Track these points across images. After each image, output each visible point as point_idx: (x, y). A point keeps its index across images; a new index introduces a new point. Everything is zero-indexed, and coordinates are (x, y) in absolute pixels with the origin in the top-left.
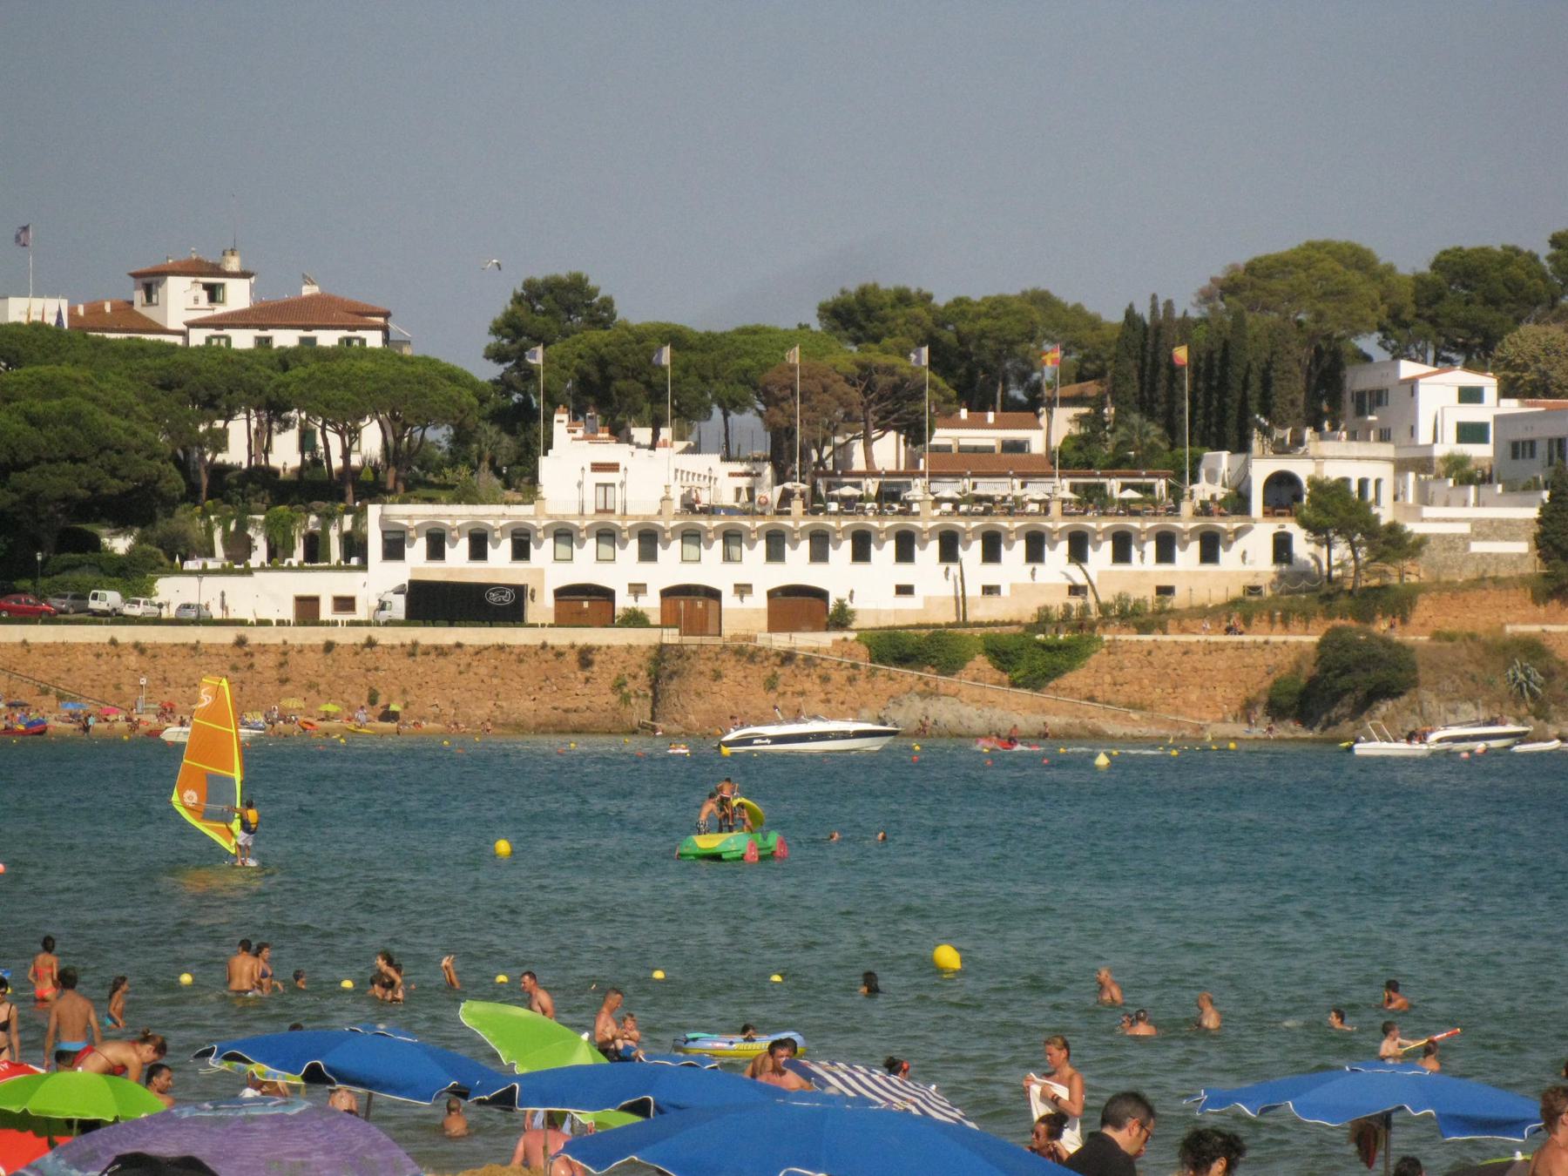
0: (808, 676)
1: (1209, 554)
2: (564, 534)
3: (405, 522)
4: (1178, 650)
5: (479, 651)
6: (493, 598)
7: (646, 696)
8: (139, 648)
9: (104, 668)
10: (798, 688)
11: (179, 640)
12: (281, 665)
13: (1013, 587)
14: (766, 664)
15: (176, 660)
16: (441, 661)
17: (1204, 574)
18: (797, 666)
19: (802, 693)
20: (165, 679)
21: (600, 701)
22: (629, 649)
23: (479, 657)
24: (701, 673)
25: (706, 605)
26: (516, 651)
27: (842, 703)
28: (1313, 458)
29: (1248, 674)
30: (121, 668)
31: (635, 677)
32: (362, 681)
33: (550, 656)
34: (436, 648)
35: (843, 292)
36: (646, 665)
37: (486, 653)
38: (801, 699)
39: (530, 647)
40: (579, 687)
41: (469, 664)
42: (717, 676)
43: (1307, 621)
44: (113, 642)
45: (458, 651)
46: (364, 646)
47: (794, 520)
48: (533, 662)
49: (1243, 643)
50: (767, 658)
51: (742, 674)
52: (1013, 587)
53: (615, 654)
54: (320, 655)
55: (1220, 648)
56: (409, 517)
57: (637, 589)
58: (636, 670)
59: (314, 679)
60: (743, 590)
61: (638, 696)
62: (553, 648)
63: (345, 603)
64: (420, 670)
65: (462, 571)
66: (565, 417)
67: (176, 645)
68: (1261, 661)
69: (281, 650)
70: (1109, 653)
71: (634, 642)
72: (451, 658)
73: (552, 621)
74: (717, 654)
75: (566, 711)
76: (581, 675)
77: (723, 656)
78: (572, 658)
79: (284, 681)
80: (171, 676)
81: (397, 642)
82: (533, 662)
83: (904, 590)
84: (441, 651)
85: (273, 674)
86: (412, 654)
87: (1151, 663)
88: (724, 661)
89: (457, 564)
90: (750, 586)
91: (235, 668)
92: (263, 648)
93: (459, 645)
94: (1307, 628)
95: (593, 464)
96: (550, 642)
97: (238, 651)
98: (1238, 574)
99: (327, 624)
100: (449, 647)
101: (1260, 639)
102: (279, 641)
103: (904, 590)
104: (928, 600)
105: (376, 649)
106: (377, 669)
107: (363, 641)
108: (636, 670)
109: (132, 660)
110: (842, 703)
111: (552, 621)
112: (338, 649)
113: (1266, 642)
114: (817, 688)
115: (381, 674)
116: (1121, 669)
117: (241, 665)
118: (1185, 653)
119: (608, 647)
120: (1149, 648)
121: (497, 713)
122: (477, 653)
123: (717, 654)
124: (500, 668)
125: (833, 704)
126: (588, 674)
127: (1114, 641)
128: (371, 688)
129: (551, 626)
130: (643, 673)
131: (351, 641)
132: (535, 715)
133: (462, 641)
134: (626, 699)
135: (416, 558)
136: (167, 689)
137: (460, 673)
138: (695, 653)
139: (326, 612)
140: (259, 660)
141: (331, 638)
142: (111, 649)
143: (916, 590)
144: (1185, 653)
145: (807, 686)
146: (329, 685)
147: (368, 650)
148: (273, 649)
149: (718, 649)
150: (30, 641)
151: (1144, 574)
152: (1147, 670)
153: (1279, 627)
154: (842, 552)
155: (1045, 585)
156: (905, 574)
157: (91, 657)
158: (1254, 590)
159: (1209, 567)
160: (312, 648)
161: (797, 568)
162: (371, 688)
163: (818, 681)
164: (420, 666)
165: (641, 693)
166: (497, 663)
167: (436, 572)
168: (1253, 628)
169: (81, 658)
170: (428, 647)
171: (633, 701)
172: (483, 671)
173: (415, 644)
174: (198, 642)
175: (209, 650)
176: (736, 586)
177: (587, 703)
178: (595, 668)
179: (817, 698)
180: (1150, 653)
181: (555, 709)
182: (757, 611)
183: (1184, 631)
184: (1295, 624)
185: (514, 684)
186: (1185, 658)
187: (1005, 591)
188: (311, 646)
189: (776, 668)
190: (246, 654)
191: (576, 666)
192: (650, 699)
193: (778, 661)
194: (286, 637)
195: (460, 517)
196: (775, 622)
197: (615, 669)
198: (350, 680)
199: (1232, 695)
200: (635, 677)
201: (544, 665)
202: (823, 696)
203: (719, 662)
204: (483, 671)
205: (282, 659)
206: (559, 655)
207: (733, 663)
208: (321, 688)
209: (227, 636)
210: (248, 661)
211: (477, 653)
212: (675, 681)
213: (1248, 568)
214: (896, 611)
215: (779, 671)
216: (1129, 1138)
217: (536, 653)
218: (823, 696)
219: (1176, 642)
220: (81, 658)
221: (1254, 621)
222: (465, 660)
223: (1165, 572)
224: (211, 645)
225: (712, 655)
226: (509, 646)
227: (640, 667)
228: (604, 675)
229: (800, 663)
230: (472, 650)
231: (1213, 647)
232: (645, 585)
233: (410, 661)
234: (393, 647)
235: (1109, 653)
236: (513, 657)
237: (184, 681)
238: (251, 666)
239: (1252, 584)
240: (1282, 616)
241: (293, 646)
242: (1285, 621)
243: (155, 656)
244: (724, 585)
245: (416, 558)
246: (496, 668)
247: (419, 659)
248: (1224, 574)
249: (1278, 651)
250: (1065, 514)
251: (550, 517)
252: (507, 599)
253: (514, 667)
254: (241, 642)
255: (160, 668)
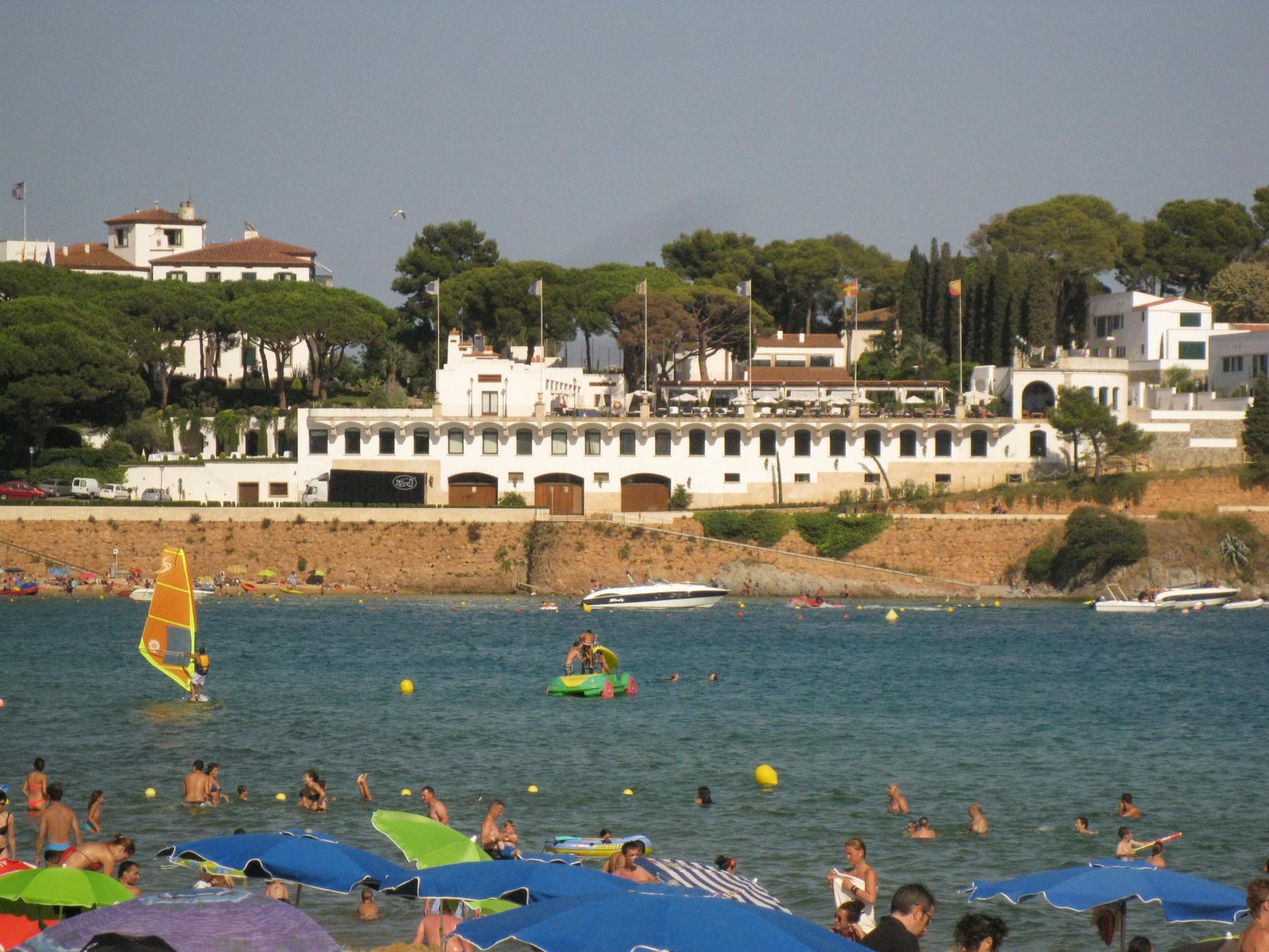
0: (654, 547)
1: (979, 448)
2: (457, 433)
3: (328, 423)
4: (954, 526)
5: (388, 527)
6: (399, 484)
7: (523, 563)
8: (113, 525)
9: (84, 540)
10: (646, 557)
11: (145, 518)
12: (228, 538)
13: (820, 475)
14: (620, 537)
15: (142, 534)
16: (357, 535)
17: (975, 465)
18: (645, 539)
19: (649, 561)
20: (133, 550)
21: (486, 568)
22: (509, 525)
23: (387, 532)
24: (568, 545)
25: (571, 490)
26: (418, 527)
27: (682, 569)
28: (1063, 371)
29: (1010, 545)
30: (98, 540)
31: (514, 548)
32: (293, 551)
33: (445, 531)
34: (353, 524)
35: (682, 237)
36: (523, 538)
37: (393, 529)
38: (648, 566)
39: (429, 524)
40: (469, 556)
41: (380, 538)
42: (581, 547)
43: (1058, 503)
44: (92, 520)
45: (371, 527)
46: (295, 523)
47: (643, 421)
48: (431, 536)
49: (1006, 520)
50: (621, 533)
51: (600, 545)
52: (820, 475)
53: (498, 529)
54: (259, 530)
55: (987, 524)
56: (331, 419)
57: (516, 477)
58: (515, 542)
59: (254, 550)
60: (601, 477)
61: (516, 564)
62: (447, 524)
63: (279, 489)
64: (340, 542)
65: (374, 462)
66: (457, 338)
67: (142, 522)
68: (1020, 535)
69: (227, 526)
70: (898, 529)
71: (513, 520)
72: (365, 532)
73: (447, 503)
74: (580, 529)
75: (458, 575)
76: (470, 547)
77: (585, 531)
78: (463, 532)
79: (229, 552)
80: (138, 547)
81: (321, 520)
82: (431, 536)
83: (732, 478)
84: (357, 527)
85: (221, 546)
86: (333, 530)
87: (931, 537)
88: (586, 535)
89: (370, 457)
90: (607, 474)
91: (190, 541)
92: (213, 525)
93: (371, 522)
94: (1058, 508)
95: (480, 376)
96: (445, 520)
97: (193, 527)
98: (1002, 465)
99: (265, 505)
100: (364, 524)
101: (1020, 517)
102: (226, 519)
103: (732, 478)
104: (751, 486)
105: (304, 525)
106: (305, 542)
107: (294, 519)
108: (515, 542)
109: (107, 534)
110: (682, 569)
111: (447, 503)
112: (273, 525)
113: (1025, 520)
114: (661, 557)
115: (309, 545)
116: (907, 542)
117: (195, 539)
118: (959, 529)
119: (492, 524)
120: (930, 524)
121: (402, 577)
122: (386, 529)
123: (580, 529)
124: (405, 541)
125: (675, 570)
126: (476, 546)
127: (902, 519)
128: (300, 557)
129: (446, 507)
130: (520, 545)
131: (284, 519)
132: (433, 579)
133: (374, 519)
134: (506, 566)
135: (337, 452)
136: (135, 558)
137: (373, 545)
138: (562, 528)
139: (264, 495)
140: (209, 534)
141: (268, 517)
142: (90, 525)
143: (741, 478)
144: (959, 529)
145: (654, 555)
146: (266, 554)
147: (297, 526)
148: (221, 525)
149: (581, 526)
150: (24, 519)
151: (926, 465)
152: (928, 543)
153: (1035, 507)
154: (682, 447)
155: (846, 474)
156: (732, 464)
157: (73, 532)
158: (1015, 478)
159: (978, 459)
160: (253, 524)
161: (645, 460)
162: (300, 557)
163: (662, 551)
164: (340, 539)
165: (519, 561)
166: (403, 537)
167: (353, 463)
168: (1014, 508)
169: (65, 533)
170: (346, 523)
171: (512, 567)
172: (391, 543)
173: (336, 522)
174: (160, 520)
175: (169, 526)
176: (596, 474)
177: (475, 569)
178: (482, 541)
179: (661, 565)
180: (930, 529)
181: (449, 574)
182: (612, 495)
183: (958, 511)
184: (1048, 505)
185: (416, 554)
186: (959, 533)
187: (813, 479)
188: (251, 523)
189: (628, 541)
190: (199, 530)
191: (466, 539)
192: (526, 566)
193: (630, 535)
194: (232, 516)
195: (372, 418)
196: (628, 504)
197: (498, 542)
198: (283, 550)
199: (997, 563)
200: (514, 548)
201: (440, 539)
202: (666, 563)
203: (582, 536)
204: (391, 543)
205: (228, 533)
206: (453, 530)
207: (593, 536)
208: (260, 557)
209: (184, 515)
210: (200, 535)
211: (386, 529)
212: (547, 551)
213: (1010, 460)
214: (725, 495)
215: (631, 543)
216: (913, 921)
217: (434, 529)
218: (666, 563)
219: (951, 520)
220: (65, 533)
221: (1015, 503)
222: (376, 534)
223: (943, 463)
224: (171, 522)
225: (577, 530)
226: (412, 523)
227: (518, 540)
228: (488, 546)
229: (648, 536)
230: (382, 526)
231: (982, 524)
232: (522, 474)
233: (332, 535)
234: (318, 524)
235: (898, 529)
236: (415, 532)
237: (149, 551)
238: (203, 539)
239: (1013, 473)
240: (1037, 499)
241: (237, 523)
242: (1040, 503)
243: (125, 531)
244: (586, 473)
245: (337, 452)
246: (401, 541)
247: (339, 533)
248: (991, 465)
249: (1034, 527)
250: (862, 416)
251: (445, 418)
252: (411, 485)
253: (416, 540)
254: (195, 520)
255: (130, 541)
